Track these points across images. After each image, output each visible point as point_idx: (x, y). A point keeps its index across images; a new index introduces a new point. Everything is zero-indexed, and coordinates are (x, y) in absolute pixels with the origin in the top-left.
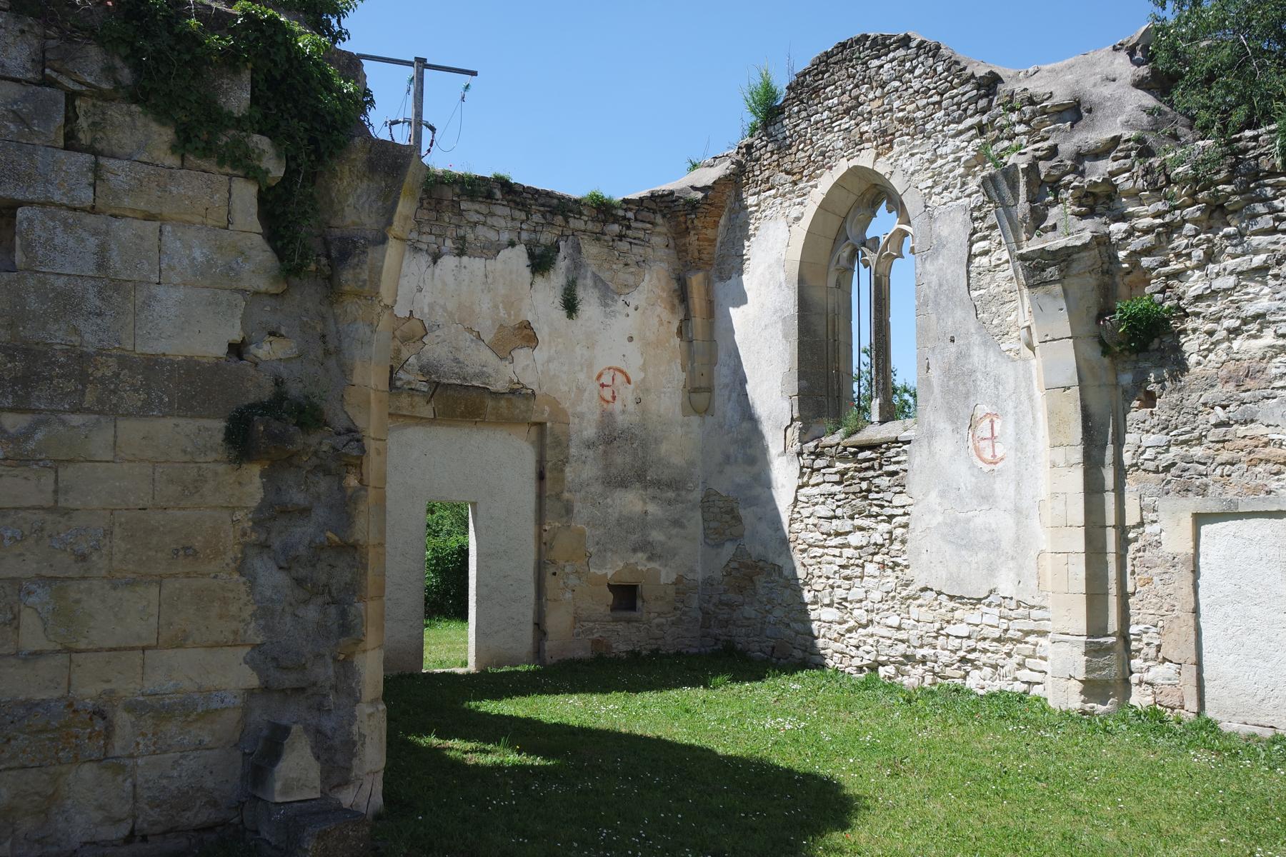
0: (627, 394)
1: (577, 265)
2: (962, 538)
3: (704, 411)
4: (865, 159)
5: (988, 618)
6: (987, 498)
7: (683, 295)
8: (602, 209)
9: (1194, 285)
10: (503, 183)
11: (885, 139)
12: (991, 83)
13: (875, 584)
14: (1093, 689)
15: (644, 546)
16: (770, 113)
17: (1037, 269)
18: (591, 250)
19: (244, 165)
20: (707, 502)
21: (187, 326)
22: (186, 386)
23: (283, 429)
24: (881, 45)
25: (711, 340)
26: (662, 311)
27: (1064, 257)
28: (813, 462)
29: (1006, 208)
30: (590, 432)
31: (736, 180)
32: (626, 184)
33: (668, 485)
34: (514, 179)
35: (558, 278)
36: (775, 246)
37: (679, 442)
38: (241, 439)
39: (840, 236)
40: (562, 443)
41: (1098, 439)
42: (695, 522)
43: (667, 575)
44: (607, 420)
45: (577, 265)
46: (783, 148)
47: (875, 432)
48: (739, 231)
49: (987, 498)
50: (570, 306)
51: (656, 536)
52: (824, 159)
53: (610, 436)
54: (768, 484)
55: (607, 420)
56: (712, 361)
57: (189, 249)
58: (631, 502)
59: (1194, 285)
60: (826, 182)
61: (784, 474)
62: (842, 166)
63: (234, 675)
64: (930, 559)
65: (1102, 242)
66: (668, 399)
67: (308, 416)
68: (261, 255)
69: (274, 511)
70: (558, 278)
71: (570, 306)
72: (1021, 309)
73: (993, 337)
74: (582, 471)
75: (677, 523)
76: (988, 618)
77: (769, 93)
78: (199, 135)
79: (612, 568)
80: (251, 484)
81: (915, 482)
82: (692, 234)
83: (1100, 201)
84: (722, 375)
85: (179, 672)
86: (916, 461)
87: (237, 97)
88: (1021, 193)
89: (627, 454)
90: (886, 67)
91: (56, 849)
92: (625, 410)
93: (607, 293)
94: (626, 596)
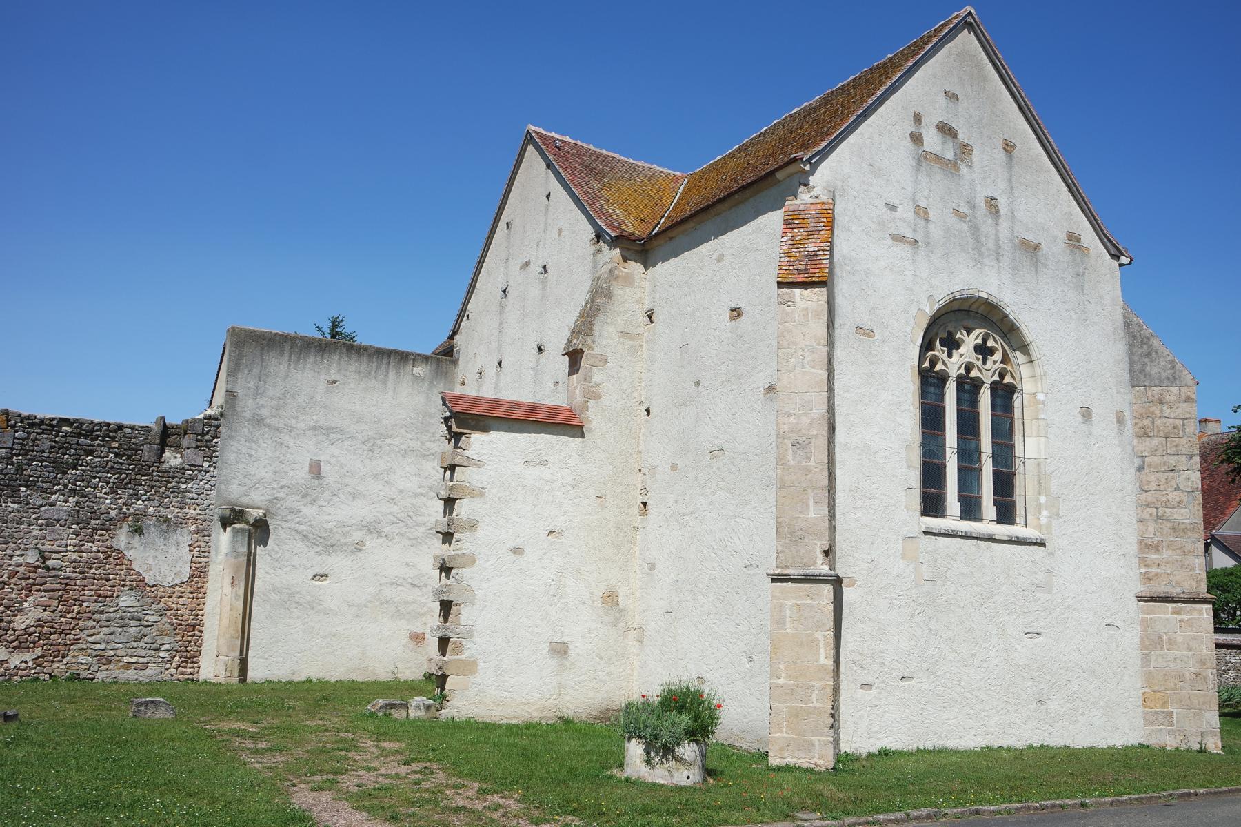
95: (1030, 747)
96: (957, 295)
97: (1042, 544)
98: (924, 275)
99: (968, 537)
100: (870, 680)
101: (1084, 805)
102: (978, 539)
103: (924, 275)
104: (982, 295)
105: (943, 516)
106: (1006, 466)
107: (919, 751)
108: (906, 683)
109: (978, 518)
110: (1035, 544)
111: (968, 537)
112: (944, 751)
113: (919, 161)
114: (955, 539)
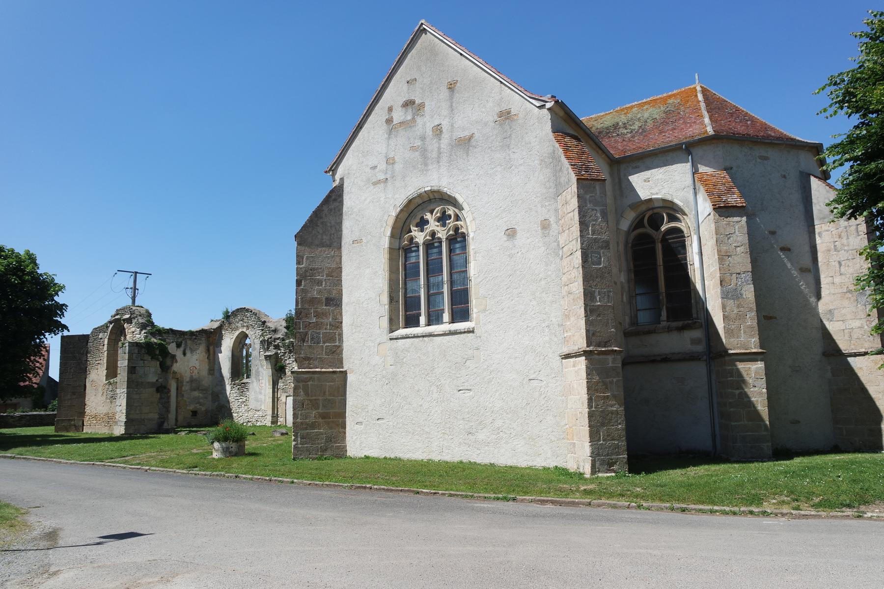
0: (196, 372)
1: (186, 345)
2: (257, 400)
3: (213, 375)
4: (244, 330)
5: (260, 413)
6: (261, 393)
7: (208, 350)
8: (191, 333)
9: (287, 362)
10: (171, 330)
11: (248, 329)
12: (264, 322)
13: (243, 408)
14: (272, 423)
15: (199, 403)
16: (227, 316)
17: (267, 358)
18: (189, 342)
19: (158, 359)
20: (212, 394)
21: (152, 379)
22: (152, 385)
23: (162, 389)
24: (248, 310)
25: (214, 359)
26: (204, 354)
27: (270, 356)
28: (233, 386)
29: (264, 346)
30: (188, 380)
31: (220, 328)
32: (195, 327)
33: (204, 390)
34: (175, 328)
35: (182, 349)
36: (228, 342)
37: (207, 381)
38: (158, 390)
39: (240, 343)
40: (182, 382)
41: (275, 384)
42: (210, 397)
43: (203, 409)
44: (192, 376)
45: (186, 345)
46: (230, 324)
47: (245, 381)
48: (221, 338)
49: (261, 393)
50: (184, 354)
51: (201, 401)
52: (237, 328)
53: (192, 380)
54: (225, 390)
55: (192, 376)
56: (214, 364)
57: (153, 370)
58: (196, 394)
59: (287, 362)
60: (237, 333)
61: (228, 388)
62: (241, 330)
63: (156, 416)
64: (252, 404)
65: (276, 354)
66: (205, 372)
67: (165, 387)
68: (159, 370)
69: (161, 398)
70: (182, 349)
71: (184, 354)
72: (265, 362)
73: (262, 366)
74: (186, 388)
75: (206, 398)
76: (260, 413)
77: (227, 312)
78: (154, 357)
79: (191, 408)
80: (158, 395)
81: (250, 390)
82: (210, 339)
83: (277, 347)
84: (216, 367)
85: (151, 416)
86: (250, 386)
87: (157, 352)
88: (266, 344)
89: (195, 384)
90: (248, 314)
91: (702, 169)
92: (195, 375)
93: (192, 351)
94: (194, 413)
95: (461, 462)
96: (410, 197)
97: (473, 332)
98: (390, 196)
99: (414, 337)
100: (360, 420)
101: (293, 482)
102: (423, 336)
103: (390, 196)
104: (427, 189)
105: (442, 323)
106: (464, 284)
107: (385, 458)
108: (380, 422)
109: (417, 324)
110: (465, 332)
111: (414, 337)
112: (397, 459)
113: (390, 132)
114: (408, 340)
